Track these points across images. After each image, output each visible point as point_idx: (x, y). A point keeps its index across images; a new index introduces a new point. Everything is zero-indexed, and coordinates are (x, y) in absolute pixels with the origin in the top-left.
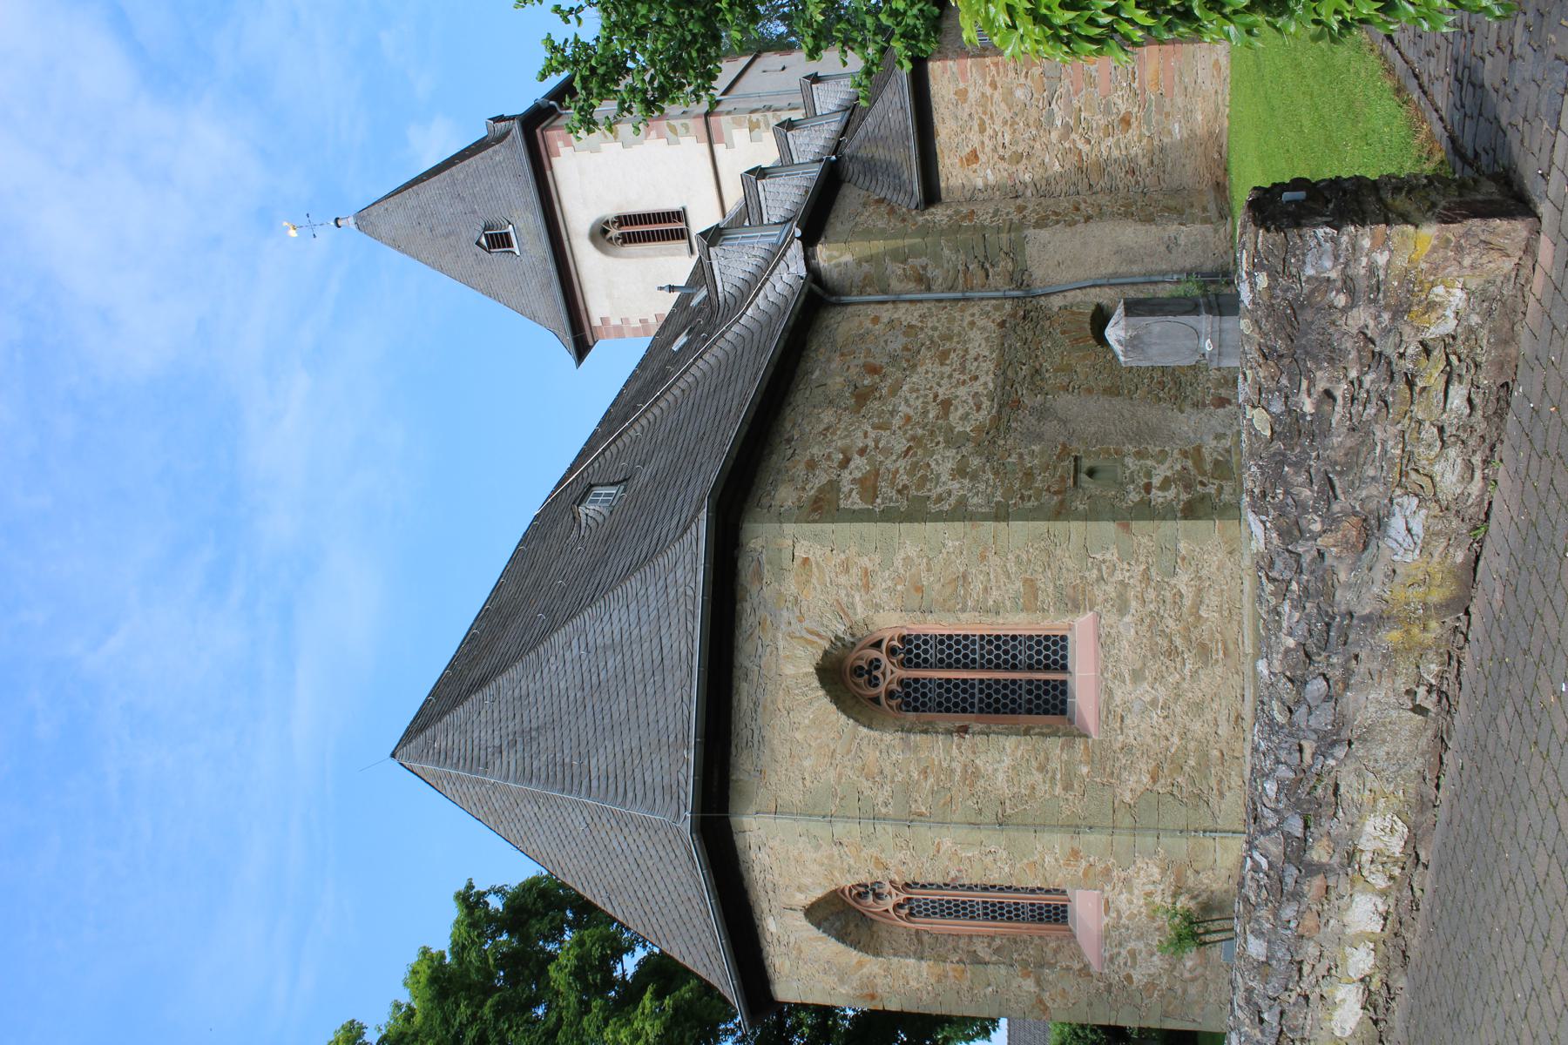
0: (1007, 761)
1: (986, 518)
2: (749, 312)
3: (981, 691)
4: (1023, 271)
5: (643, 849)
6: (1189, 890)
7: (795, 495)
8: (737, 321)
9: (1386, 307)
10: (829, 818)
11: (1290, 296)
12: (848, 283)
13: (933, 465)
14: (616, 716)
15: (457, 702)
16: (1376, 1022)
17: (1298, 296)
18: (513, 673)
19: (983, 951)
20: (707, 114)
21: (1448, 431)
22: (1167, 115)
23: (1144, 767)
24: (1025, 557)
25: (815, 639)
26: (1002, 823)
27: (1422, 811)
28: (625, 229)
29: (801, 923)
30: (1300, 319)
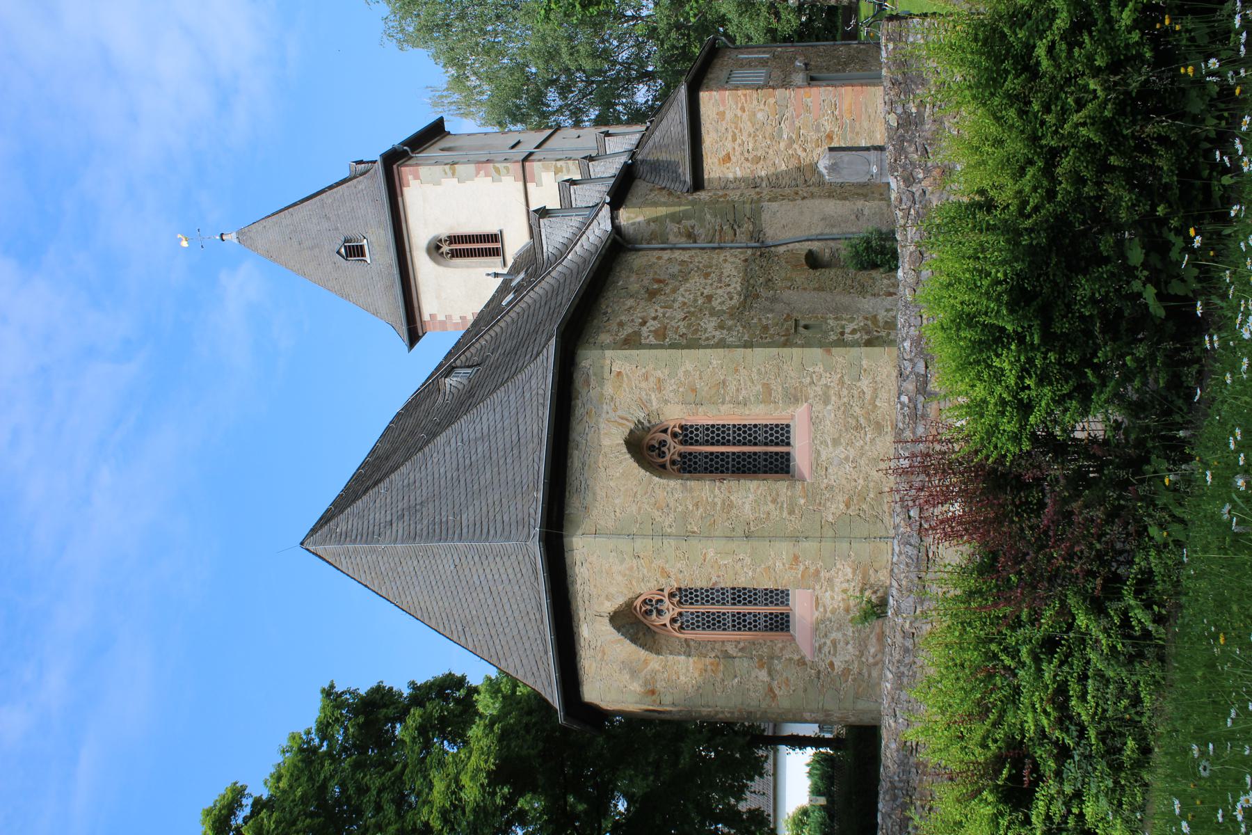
0: (751, 497)
2: (569, 257)
4: (760, 231)
5: (496, 577)
6: (871, 586)
10: (632, 536)
12: (639, 237)
15: (357, 497)
18: (403, 469)
19: (731, 650)
20: (525, 159)
28: (454, 247)
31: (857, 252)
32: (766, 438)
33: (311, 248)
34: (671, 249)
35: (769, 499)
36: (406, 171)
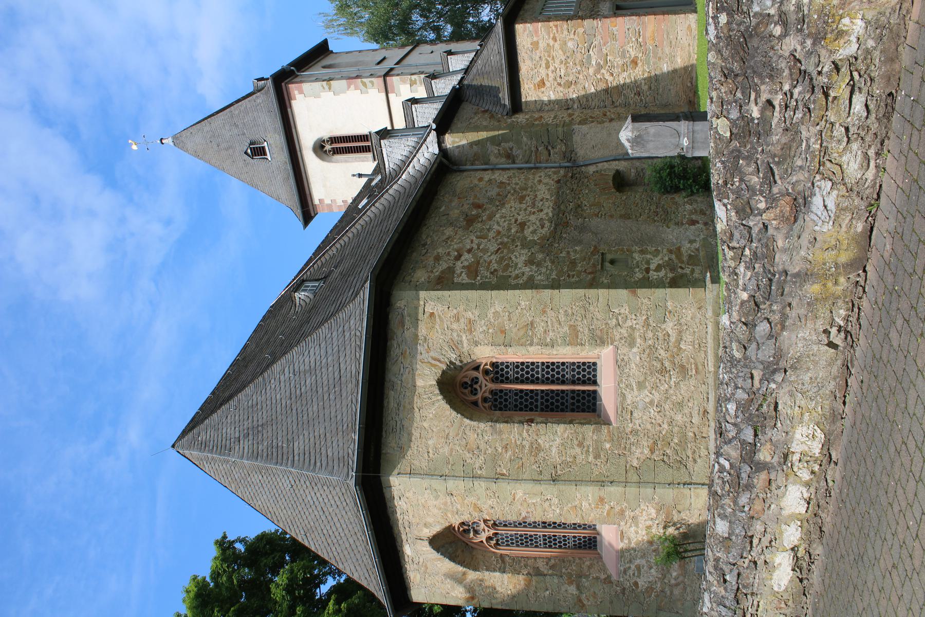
0: (558, 441)
1: (545, 287)
2: (404, 177)
3: (542, 398)
5: (326, 501)
7: (426, 275)
8: (396, 182)
9: (809, 35)
11: (742, 28)
13: (513, 258)
14: (311, 414)
15: (213, 411)
16: (801, 580)
17: (747, 28)
18: (248, 390)
20: (387, 74)
21: (852, 130)
22: (660, 58)
23: (645, 444)
24: (570, 311)
25: (438, 363)
27: (833, 422)
28: (335, 146)
30: (749, 45)
31: (661, 177)
32: (573, 376)
34: (492, 169)
35: (576, 442)
36: (292, 87)
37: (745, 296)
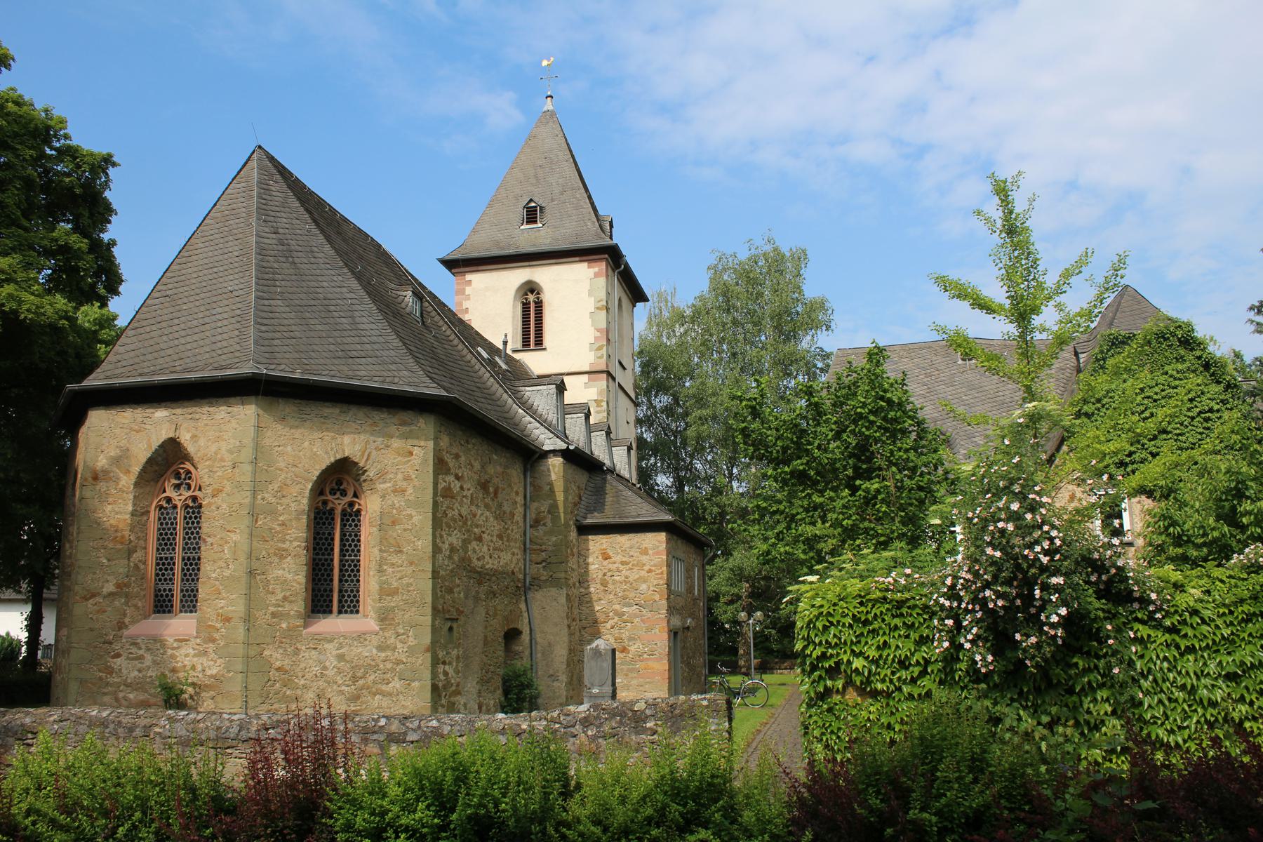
0: (290, 577)
6: (197, 694)
10: (255, 462)
18: (327, 247)
19: (137, 556)
26: (251, 573)
29: (165, 434)
33: (536, 177)
37: (524, 727)
